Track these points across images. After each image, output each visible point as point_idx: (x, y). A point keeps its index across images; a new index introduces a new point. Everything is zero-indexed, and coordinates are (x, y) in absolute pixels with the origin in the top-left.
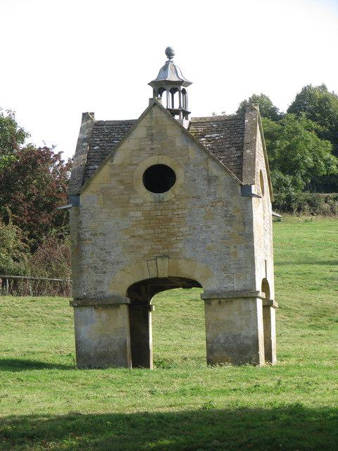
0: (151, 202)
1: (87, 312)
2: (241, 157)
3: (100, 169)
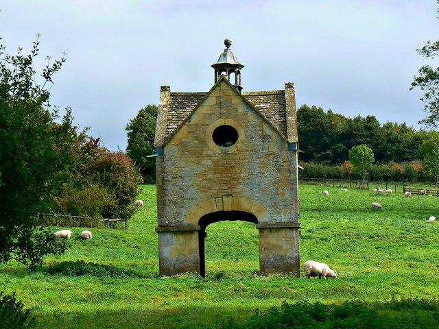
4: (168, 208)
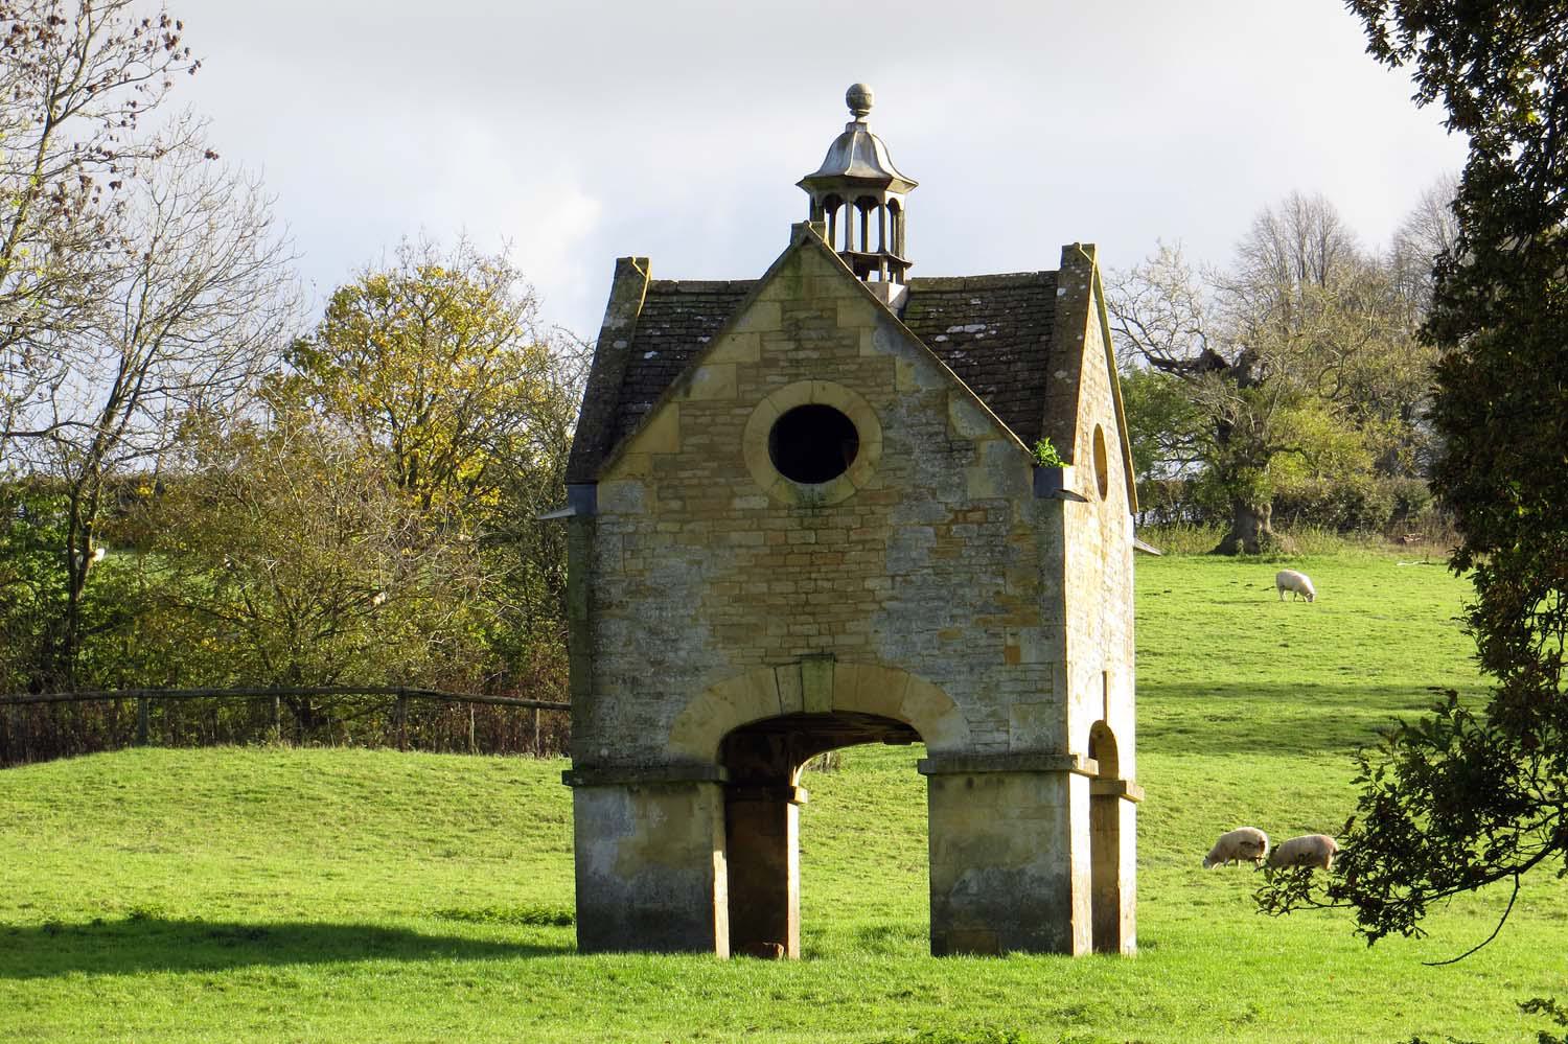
0: (789, 507)
1: (610, 801)
2: (1040, 390)
3: (655, 413)
4: (608, 700)
